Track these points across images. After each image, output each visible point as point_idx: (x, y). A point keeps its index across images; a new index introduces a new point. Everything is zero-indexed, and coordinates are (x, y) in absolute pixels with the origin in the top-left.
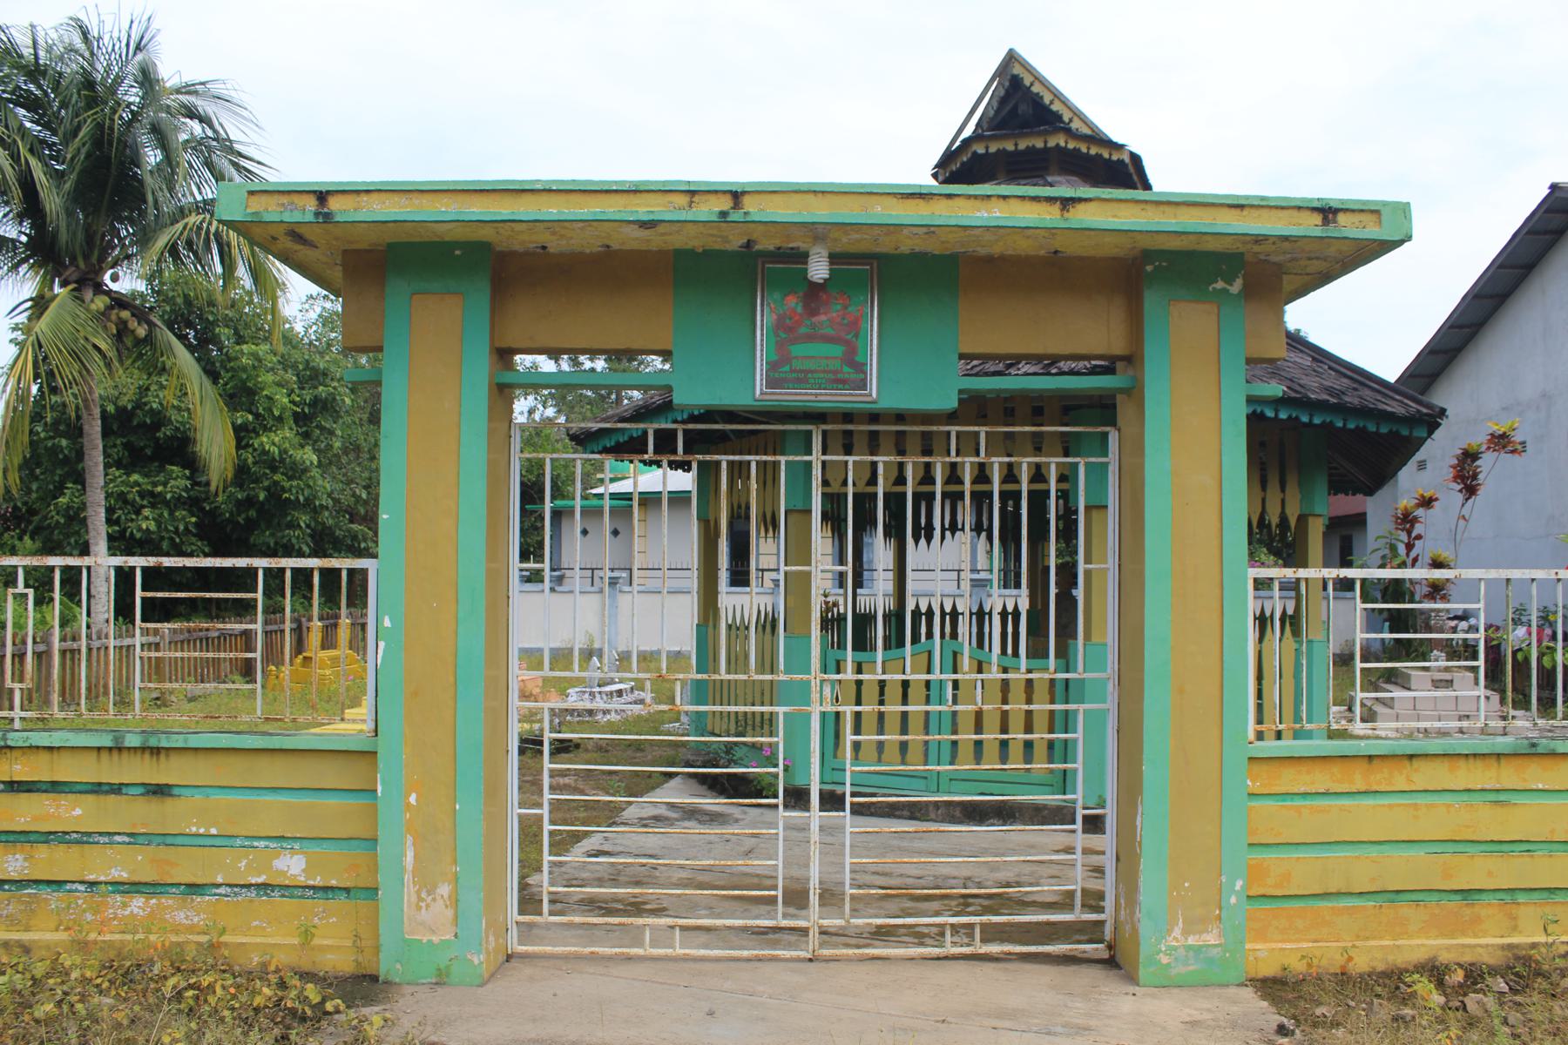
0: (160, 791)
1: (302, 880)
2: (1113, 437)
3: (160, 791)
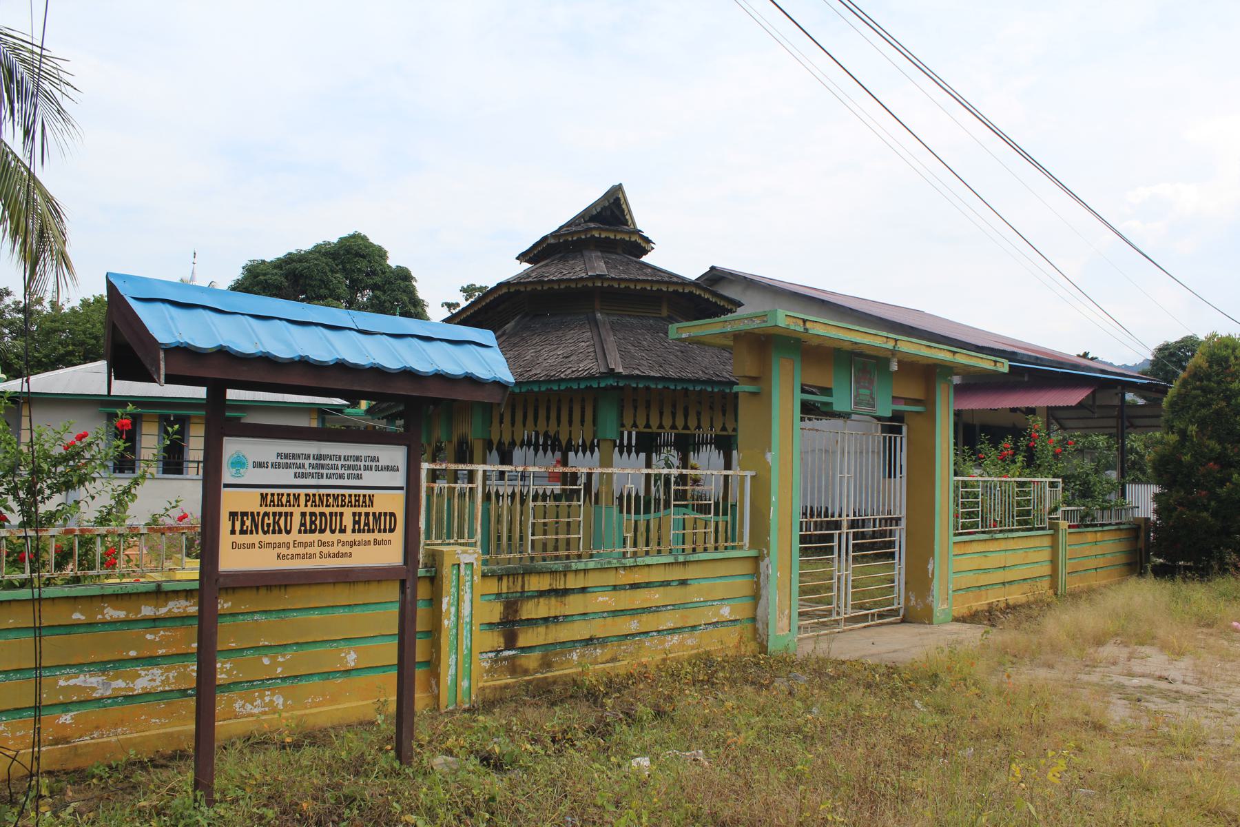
0: (683, 582)
1: (729, 618)
2: (904, 429)
3: (683, 582)
